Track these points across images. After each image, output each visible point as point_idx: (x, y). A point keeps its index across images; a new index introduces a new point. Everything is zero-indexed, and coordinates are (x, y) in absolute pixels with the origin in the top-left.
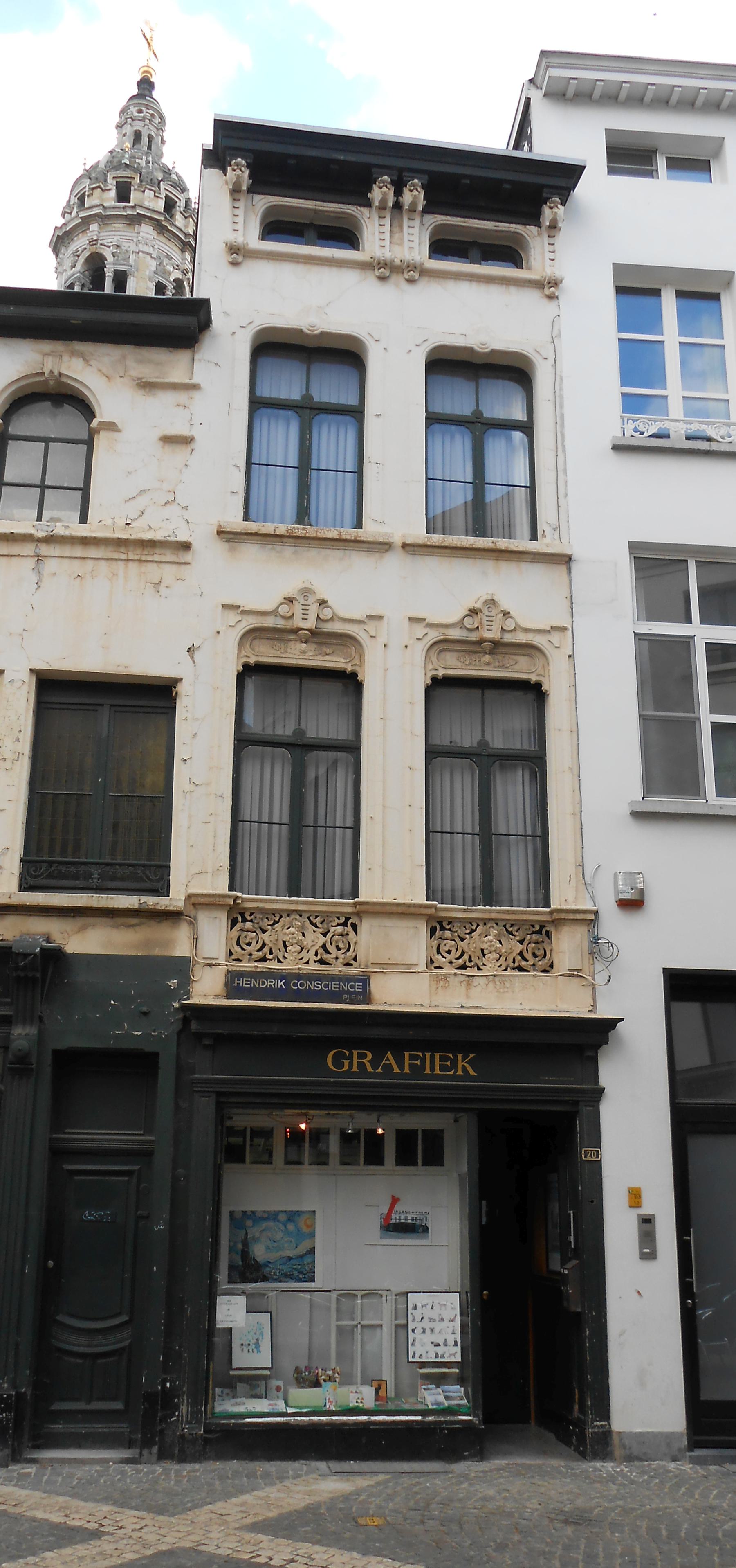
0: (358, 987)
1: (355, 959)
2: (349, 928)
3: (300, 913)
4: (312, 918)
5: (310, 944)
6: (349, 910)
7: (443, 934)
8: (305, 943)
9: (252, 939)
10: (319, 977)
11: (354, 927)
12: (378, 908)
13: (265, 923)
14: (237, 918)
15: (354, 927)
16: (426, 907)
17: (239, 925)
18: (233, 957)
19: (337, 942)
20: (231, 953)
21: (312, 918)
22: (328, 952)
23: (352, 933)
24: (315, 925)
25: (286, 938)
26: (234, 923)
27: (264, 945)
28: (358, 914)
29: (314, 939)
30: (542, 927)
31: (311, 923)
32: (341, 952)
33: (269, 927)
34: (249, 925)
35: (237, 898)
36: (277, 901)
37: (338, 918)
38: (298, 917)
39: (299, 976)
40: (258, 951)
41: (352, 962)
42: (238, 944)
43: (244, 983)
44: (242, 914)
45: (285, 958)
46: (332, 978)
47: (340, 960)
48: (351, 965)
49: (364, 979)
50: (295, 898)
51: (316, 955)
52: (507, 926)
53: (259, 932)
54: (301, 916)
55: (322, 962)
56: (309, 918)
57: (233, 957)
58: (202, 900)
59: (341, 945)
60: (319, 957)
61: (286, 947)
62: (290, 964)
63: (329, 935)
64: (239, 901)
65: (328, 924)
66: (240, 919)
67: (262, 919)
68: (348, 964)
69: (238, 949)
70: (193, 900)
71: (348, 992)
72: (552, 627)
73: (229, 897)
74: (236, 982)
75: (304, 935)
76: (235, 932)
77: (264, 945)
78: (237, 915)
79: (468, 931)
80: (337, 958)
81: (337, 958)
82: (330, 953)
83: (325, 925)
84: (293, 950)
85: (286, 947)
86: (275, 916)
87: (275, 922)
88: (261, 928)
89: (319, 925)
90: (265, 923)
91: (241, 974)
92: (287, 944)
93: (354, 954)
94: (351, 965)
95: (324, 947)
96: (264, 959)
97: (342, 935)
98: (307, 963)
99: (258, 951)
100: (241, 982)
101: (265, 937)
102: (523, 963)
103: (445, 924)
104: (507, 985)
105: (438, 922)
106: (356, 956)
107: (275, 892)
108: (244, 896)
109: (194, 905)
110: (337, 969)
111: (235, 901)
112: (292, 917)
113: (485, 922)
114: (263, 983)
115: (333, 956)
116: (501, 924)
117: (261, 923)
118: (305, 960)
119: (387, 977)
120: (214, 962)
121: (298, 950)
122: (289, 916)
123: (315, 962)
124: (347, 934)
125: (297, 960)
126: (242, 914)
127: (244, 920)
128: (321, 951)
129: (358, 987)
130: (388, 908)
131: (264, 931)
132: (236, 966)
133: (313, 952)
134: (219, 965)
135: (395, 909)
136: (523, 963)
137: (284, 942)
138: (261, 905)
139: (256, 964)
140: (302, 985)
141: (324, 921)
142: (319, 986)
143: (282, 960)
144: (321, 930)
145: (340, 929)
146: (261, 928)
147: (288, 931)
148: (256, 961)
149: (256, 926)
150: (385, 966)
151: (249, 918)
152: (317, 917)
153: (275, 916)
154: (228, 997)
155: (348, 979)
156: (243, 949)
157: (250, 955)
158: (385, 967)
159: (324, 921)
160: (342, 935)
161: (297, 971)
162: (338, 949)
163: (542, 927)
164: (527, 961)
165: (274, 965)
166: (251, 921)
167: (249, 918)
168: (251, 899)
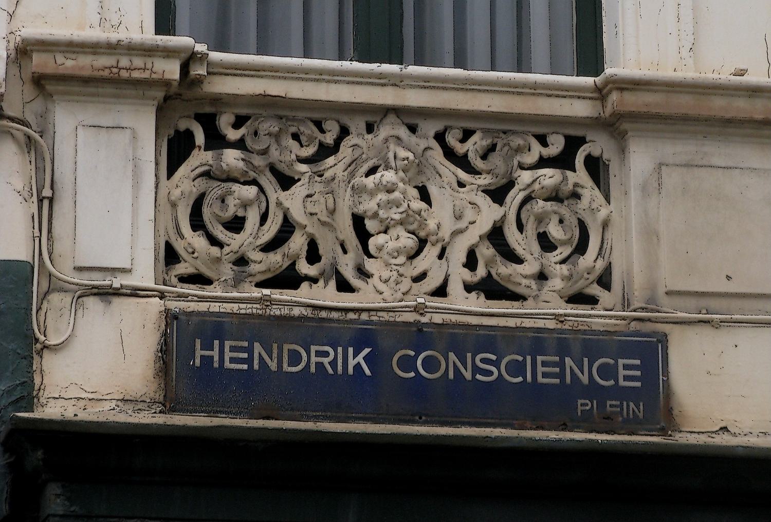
0: (627, 372)
1: (604, 281)
2: (580, 176)
3: (411, 118)
4: (455, 138)
5: (448, 227)
6: (581, 109)
7: (219, 158)
8: (432, 224)
9: (245, 205)
10: (488, 340)
11: (596, 168)
12: (684, 104)
13: (289, 153)
14: (189, 134)
15: (596, 168)
16: (148, 51)
17: (200, 158)
18: (182, 268)
19: (540, 219)
20: (171, 256)
21: (455, 138)
22: (513, 257)
23: (590, 192)
24: (462, 162)
25: (368, 205)
26: (177, 150)
27: (287, 228)
28: (616, 126)
29: (461, 211)
30: (573, 143)
31: (449, 154)
32: (554, 257)
33: (303, 168)
34: (232, 158)
35: (189, 60)
36: (333, 77)
37: (543, 140)
38: (403, 132)
39: (420, 335)
40: (270, 247)
41: (595, 290)
42: (197, 223)
43: (228, 356)
44: (209, 122)
45: (363, 273)
46: (536, 342)
47: (556, 283)
48: (592, 301)
49: (650, 352)
50: (394, 68)
51: (471, 262)
52: (452, 140)
53: (268, 182)
54: (413, 129)
55: (492, 289)
56: (440, 137)
57: (182, 268)
58: (68, 64)
59: (555, 232)
60: (481, 272)
61: (363, 236)
62: (382, 292)
63: (515, 197)
64: (199, 70)
65: (508, 158)
66: (200, 138)
67: (277, 137)
68: (580, 298)
69: (199, 241)
70: (40, 62)
71: (593, 390)
72: (470, 223)
73: (169, 53)
74: (199, 353)
75: (425, 196)
76: (185, 181)
77: (287, 228)
78: (190, 121)
79: (309, 151)
80: (542, 277)
81: (542, 277)
82: (519, 261)
83: (496, 160)
84: (392, 245)
85: (363, 236)
86: (327, 129)
87: (326, 151)
88: (273, 169)
89: (479, 164)
90: (289, 153)
91: (214, 328)
92: (370, 225)
93: (600, 265)
94: (592, 301)
95: (496, 235)
96: (288, 279)
97: (555, 196)
98: (441, 291)
99: (270, 247)
100: (215, 354)
101: (293, 201)
102: (504, 269)
103: (225, 123)
104: (160, 374)
105: (199, 118)
106: (608, 270)
107: (449, 58)
108: (215, 56)
109: (40, 82)
110: (546, 309)
111: (185, 69)
112: (384, 131)
113: (374, 117)
114: (295, 358)
115: (530, 267)
116: (430, 128)
117: (275, 154)
118: (433, 282)
119: (724, 338)
120: (117, 282)
121: (410, 249)
122: (370, 128)
123: (469, 288)
124: (576, 196)
125: (406, 284)
126: (209, 122)
127: (216, 141)
128: (486, 252)
129: (627, 372)
130: (718, 105)
131: (286, 182)
132: (194, 301)
133: (458, 254)
134: (135, 293)
135: (742, 107)
136: (504, 269)
137: (358, 221)
138: (275, 88)
139: (267, 292)
140: (430, 365)
141: (492, 148)
142: (492, 370)
143: (355, 282)
144: (484, 180)
145: (549, 177)
146: (273, 169)
147: (377, 179)
148: (260, 285)
149: (258, 161)
150: (713, 303)
151: (233, 135)
152: (467, 134)
153: (327, 129)
154: (170, 404)
155: (592, 345)
156: (214, 241)
157: (241, 261)
158: (716, 311)
159: (492, 148)
160: (555, 196)
161: (410, 317)
162: (546, 243)
163: (573, 143)
164: (519, 261)
165: (326, 295)
166: (240, 144)
167: (233, 135)
168: (243, 74)
